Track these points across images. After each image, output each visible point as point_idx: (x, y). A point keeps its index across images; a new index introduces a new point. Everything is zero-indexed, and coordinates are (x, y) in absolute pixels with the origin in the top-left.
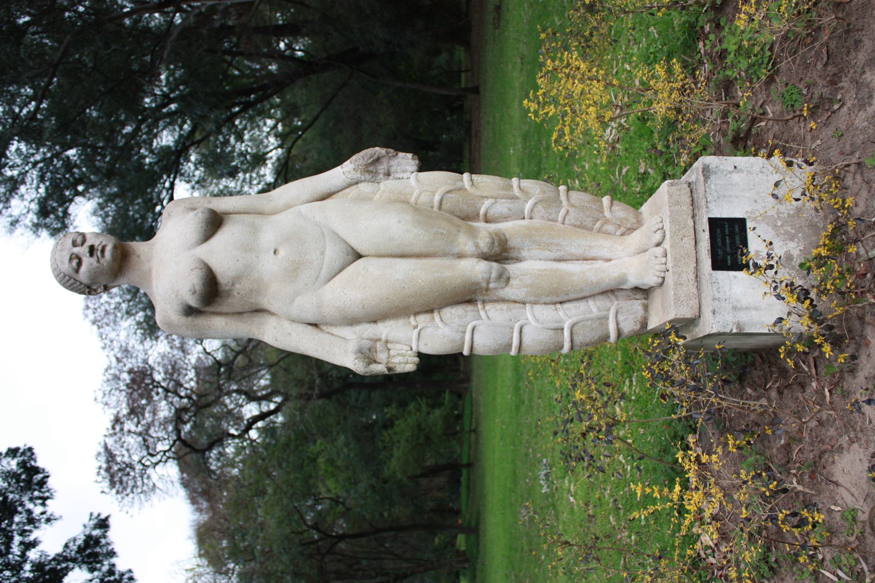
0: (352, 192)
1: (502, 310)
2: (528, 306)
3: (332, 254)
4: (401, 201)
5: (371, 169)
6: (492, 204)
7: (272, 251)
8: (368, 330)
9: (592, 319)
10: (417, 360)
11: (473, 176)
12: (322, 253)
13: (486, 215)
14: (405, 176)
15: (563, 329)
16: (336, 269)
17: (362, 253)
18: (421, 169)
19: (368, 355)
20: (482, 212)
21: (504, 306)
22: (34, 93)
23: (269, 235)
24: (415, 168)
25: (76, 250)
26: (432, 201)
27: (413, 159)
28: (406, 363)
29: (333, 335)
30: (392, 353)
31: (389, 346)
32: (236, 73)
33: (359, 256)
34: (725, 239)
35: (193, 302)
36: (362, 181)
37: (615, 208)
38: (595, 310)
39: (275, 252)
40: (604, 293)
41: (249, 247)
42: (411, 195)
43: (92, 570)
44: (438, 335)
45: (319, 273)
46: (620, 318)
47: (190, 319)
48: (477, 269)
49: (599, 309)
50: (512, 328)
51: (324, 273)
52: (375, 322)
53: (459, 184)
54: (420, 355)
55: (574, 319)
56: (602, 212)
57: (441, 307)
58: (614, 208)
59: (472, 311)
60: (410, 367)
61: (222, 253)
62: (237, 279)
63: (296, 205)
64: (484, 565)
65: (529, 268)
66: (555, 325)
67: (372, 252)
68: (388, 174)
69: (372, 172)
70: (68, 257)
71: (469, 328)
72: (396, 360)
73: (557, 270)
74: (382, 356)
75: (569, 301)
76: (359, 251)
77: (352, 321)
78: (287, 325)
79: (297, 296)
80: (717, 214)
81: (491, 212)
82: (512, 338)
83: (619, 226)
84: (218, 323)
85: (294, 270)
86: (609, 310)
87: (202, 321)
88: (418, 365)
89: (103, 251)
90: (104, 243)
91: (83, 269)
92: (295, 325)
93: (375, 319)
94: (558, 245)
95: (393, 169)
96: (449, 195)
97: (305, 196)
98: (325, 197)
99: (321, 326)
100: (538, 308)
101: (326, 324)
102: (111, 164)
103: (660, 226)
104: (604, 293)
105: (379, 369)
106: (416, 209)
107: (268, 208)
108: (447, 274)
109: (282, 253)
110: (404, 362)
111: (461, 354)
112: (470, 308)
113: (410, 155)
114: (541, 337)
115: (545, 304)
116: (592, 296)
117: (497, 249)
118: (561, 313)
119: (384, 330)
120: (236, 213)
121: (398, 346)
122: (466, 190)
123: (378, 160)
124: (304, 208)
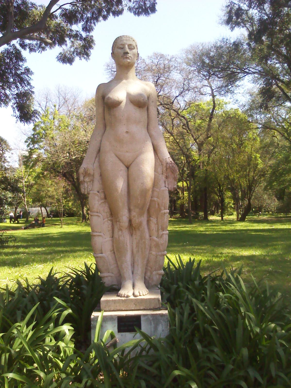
1: (108, 227)
2: (111, 239)
3: (128, 156)
7: (127, 131)
12: (127, 152)
14: (166, 185)
15: (102, 253)
21: (110, 228)
24: (170, 189)
28: (84, 189)
34: (249, 323)
38: (112, 267)
39: (127, 132)
43: (19, 57)
50: (101, 232)
53: (163, 208)
59: (107, 215)
65: (126, 238)
71: (99, 214)
73: (127, 251)
74: (87, 179)
75: (115, 256)
94: (138, 251)
102: (286, 30)
103: (142, 294)
112: (108, 214)
115: (113, 246)
116: (118, 266)
120: (148, 115)
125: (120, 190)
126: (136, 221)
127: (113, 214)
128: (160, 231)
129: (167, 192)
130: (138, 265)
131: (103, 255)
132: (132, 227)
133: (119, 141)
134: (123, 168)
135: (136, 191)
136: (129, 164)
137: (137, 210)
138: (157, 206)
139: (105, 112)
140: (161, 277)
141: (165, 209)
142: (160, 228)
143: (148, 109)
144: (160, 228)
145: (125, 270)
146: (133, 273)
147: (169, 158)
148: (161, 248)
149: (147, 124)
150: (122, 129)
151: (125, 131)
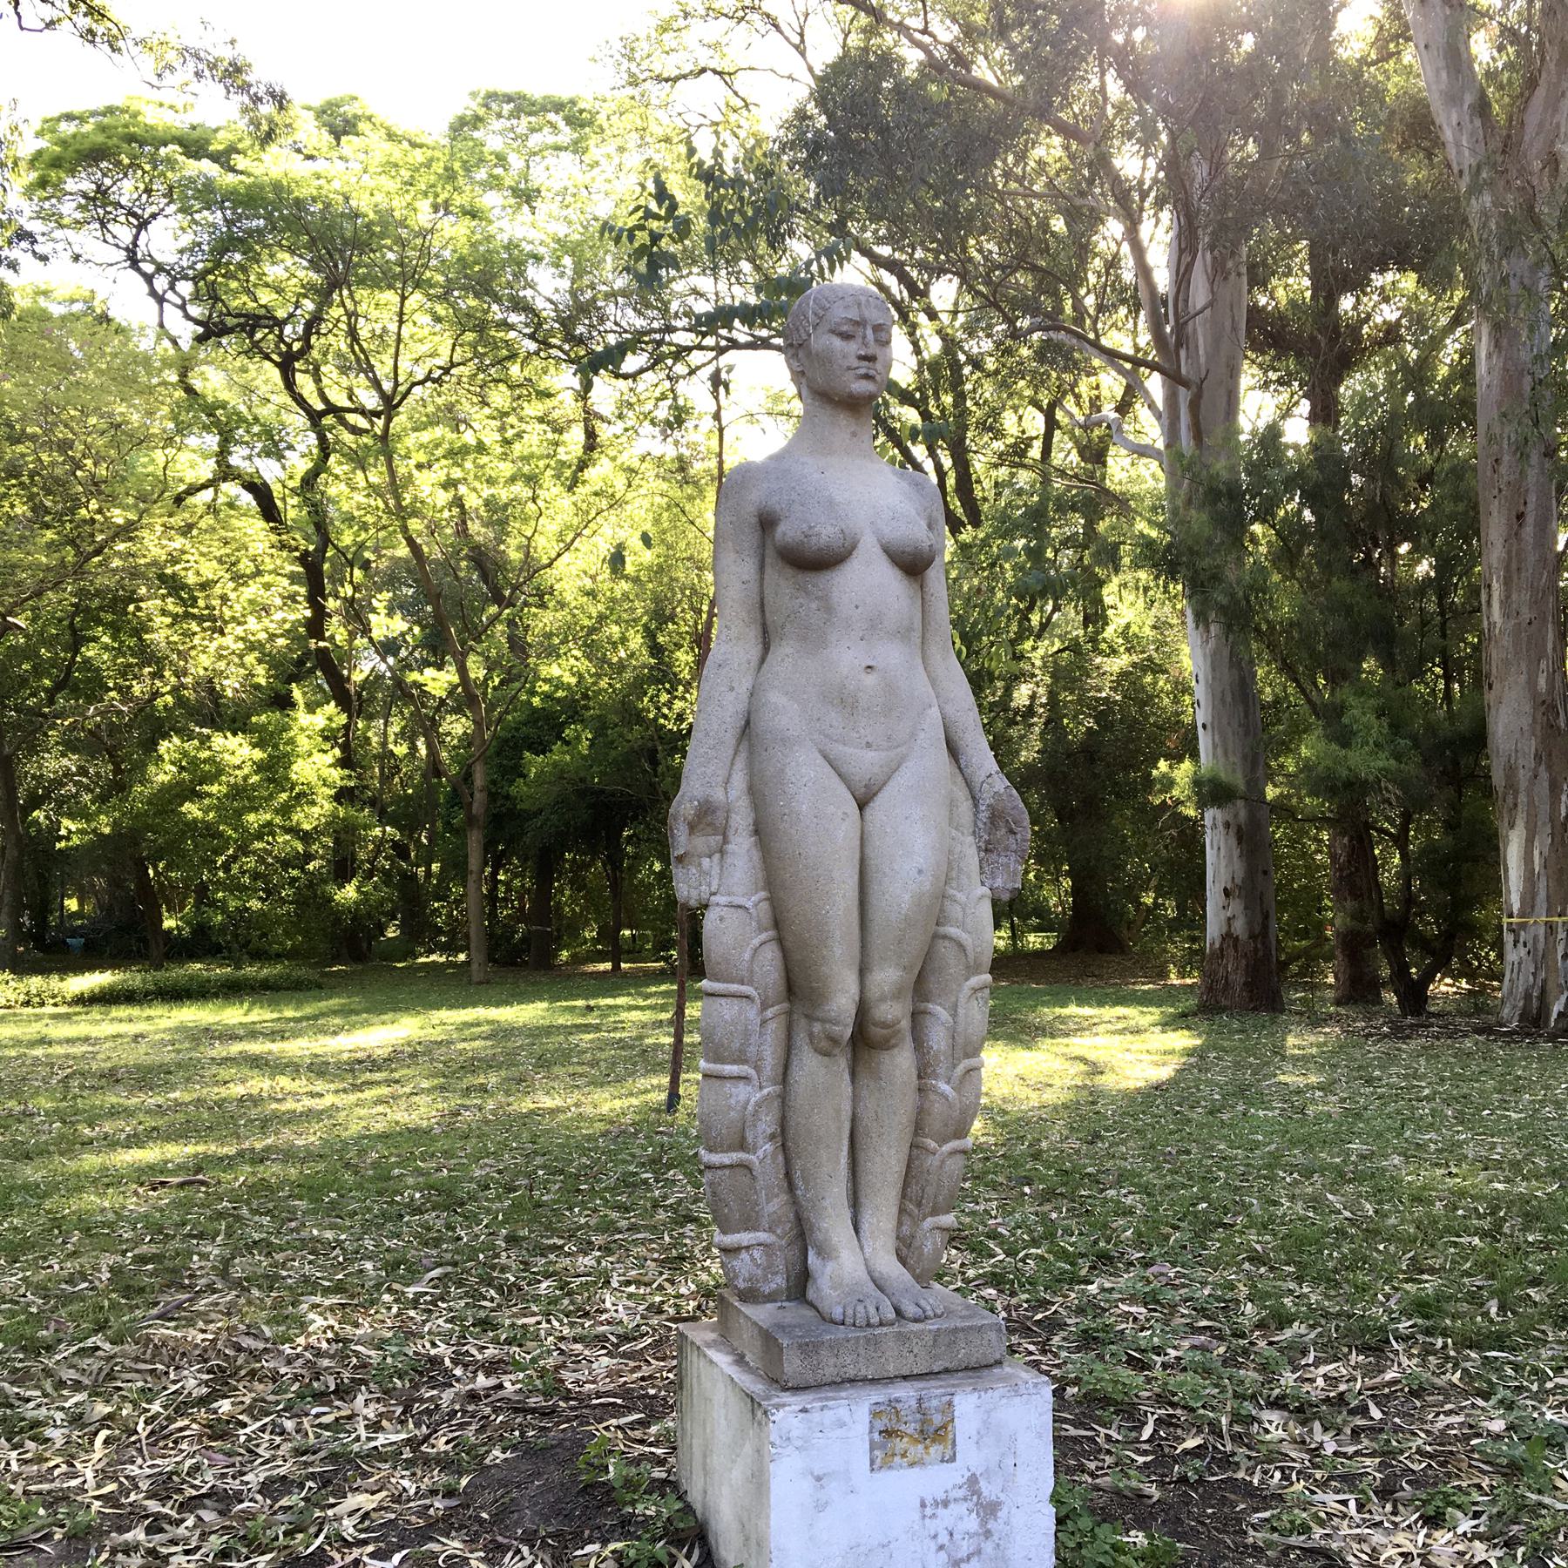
0: (961, 793)
2: (778, 1088)
3: (865, 762)
4: (949, 873)
8: (741, 820)
13: (925, 1012)
17: (868, 811)
19: (707, 817)
23: (892, 655)
30: (706, 862)
32: (1410, 399)
35: (787, 531)
36: (976, 806)
40: (957, 761)
47: (754, 520)
51: (837, 749)
52: (757, 832)
57: (780, 941)
58: (938, 1234)
61: (869, 580)
62: (828, 608)
67: (870, 828)
74: (701, 842)
77: (756, 794)
78: (744, 686)
81: (928, 1021)
84: (742, 569)
85: (845, 701)
87: (750, 539)
89: (867, 377)
91: (837, 342)
92: (745, 697)
93: (760, 831)
97: (950, 710)
98: (953, 750)
99: (744, 746)
101: (751, 752)
104: (957, 761)
107: (934, 650)
109: (870, 680)
116: (794, 1201)
117: (876, 1032)
118: (768, 1147)
119: (742, 844)
121: (716, 871)
124: (934, 712)
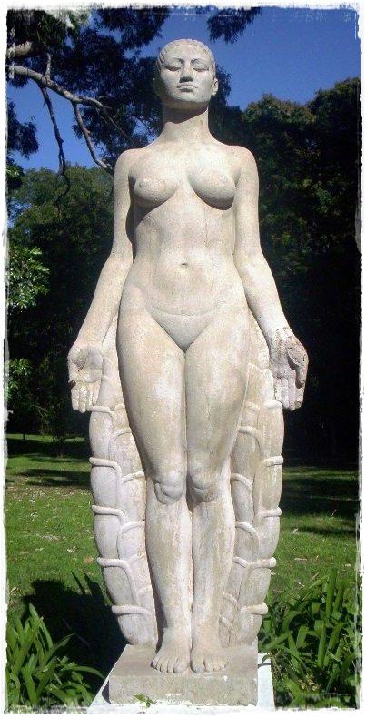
5: (277, 357)
6: (247, 487)
7: (185, 261)
9: (130, 588)
10: (83, 410)
11: (281, 467)
12: (183, 313)
14: (278, 395)
15: (119, 557)
16: (169, 327)
18: (287, 412)
20: (240, 476)
22: (30, 41)
24: (287, 406)
25: (188, 63)
26: (248, 424)
27: (296, 403)
28: (80, 400)
29: (109, 326)
30: (91, 386)
31: (98, 383)
33: (184, 349)
37: (252, 618)
41: (189, 235)
42: (255, 402)
44: (109, 434)
45: (163, 310)
46: (135, 617)
48: (173, 471)
49: (143, 596)
53: (267, 452)
54: (88, 414)
55: (129, 570)
56: (246, 604)
60: (76, 404)
63: (243, 282)
64: (155, 437)
65: (181, 523)
66: (121, 548)
68: (279, 377)
69: (279, 360)
70: (180, 57)
71: (112, 463)
72: (83, 389)
76: (192, 346)
79: (142, 290)
80: (349, 712)
82: (106, 506)
83: (232, 622)
86: (142, 606)
88: (78, 412)
89: (188, 91)
90: (195, 90)
93: (121, 368)
95: (286, 382)
96: (254, 442)
98: (252, 307)
100: (141, 532)
105: (74, 374)
106: (236, 406)
108: (164, 441)
109: (183, 272)
110: (81, 398)
111: (92, 455)
113: (301, 399)
114: (107, 536)
119: (113, 378)
122: (261, 459)
123: (293, 366)
125: (172, 405)
126: (202, 478)
127: (149, 467)
128: (260, 508)
129: (280, 412)
130: (204, 591)
131: (122, 561)
132: (195, 497)
133: (165, 285)
134: (174, 351)
135: (204, 413)
136: (187, 342)
137: (205, 456)
138: (254, 446)
139: (77, 586)
140: (261, 619)
141: (272, 455)
142: (260, 500)
143: (236, 213)
144: (260, 500)
145: (172, 602)
146: (192, 610)
147: (284, 328)
148: (262, 549)
149: (167, 335)
150: (172, 259)
151: (181, 261)
